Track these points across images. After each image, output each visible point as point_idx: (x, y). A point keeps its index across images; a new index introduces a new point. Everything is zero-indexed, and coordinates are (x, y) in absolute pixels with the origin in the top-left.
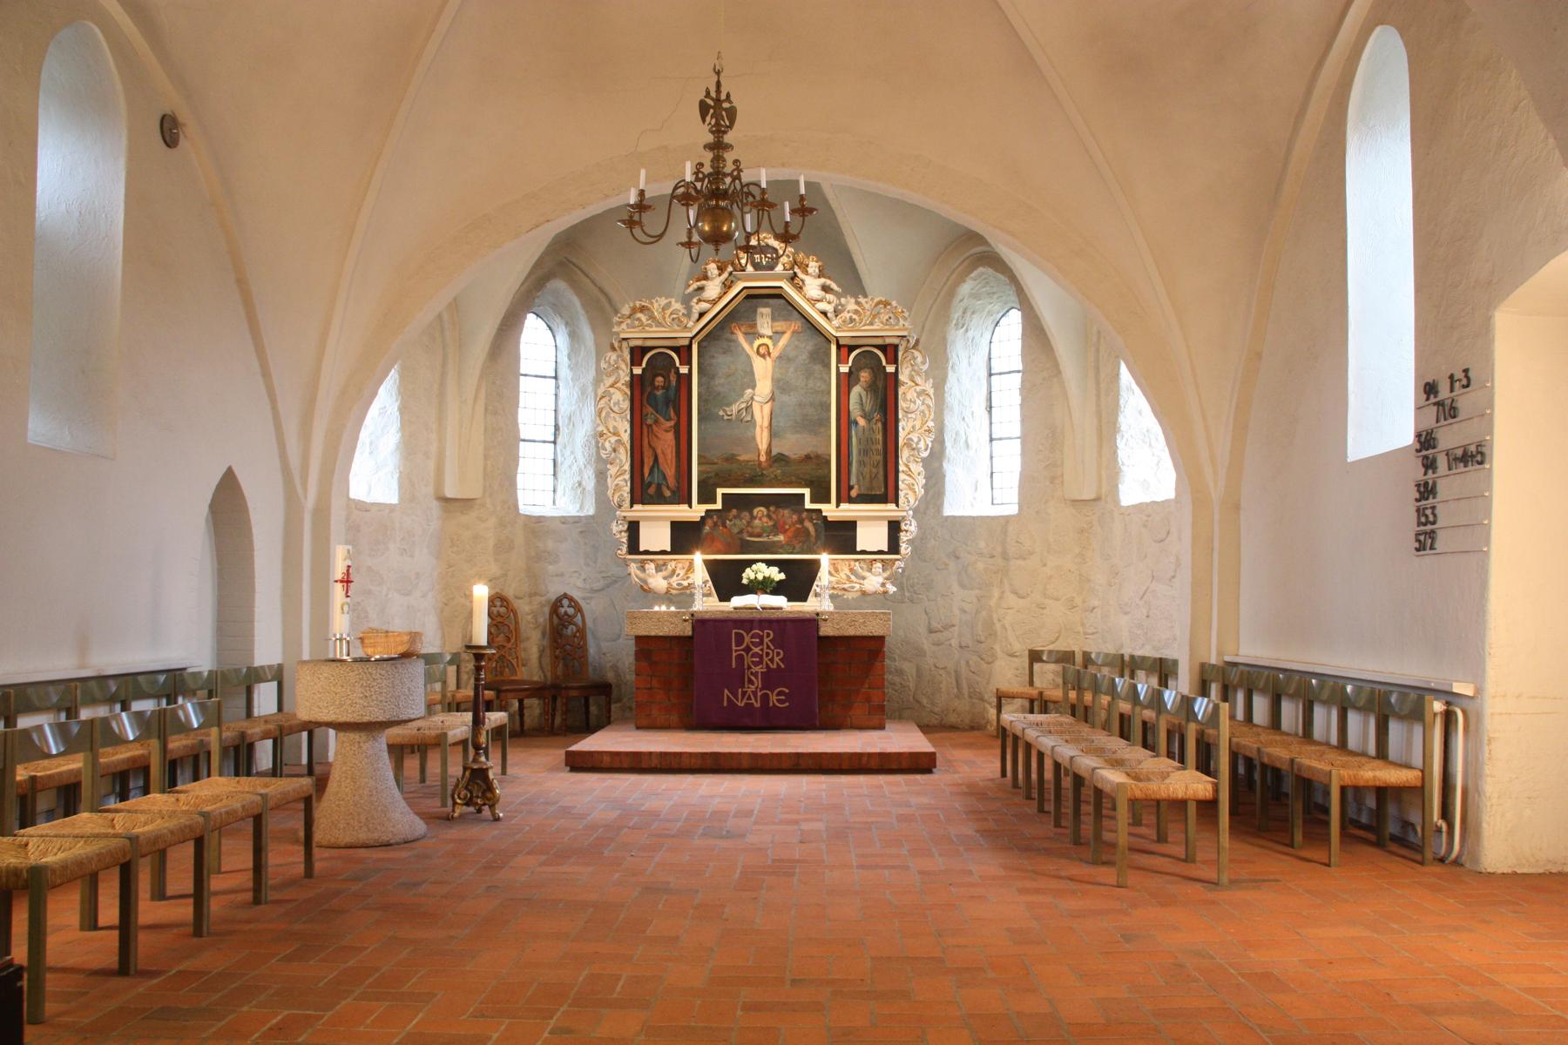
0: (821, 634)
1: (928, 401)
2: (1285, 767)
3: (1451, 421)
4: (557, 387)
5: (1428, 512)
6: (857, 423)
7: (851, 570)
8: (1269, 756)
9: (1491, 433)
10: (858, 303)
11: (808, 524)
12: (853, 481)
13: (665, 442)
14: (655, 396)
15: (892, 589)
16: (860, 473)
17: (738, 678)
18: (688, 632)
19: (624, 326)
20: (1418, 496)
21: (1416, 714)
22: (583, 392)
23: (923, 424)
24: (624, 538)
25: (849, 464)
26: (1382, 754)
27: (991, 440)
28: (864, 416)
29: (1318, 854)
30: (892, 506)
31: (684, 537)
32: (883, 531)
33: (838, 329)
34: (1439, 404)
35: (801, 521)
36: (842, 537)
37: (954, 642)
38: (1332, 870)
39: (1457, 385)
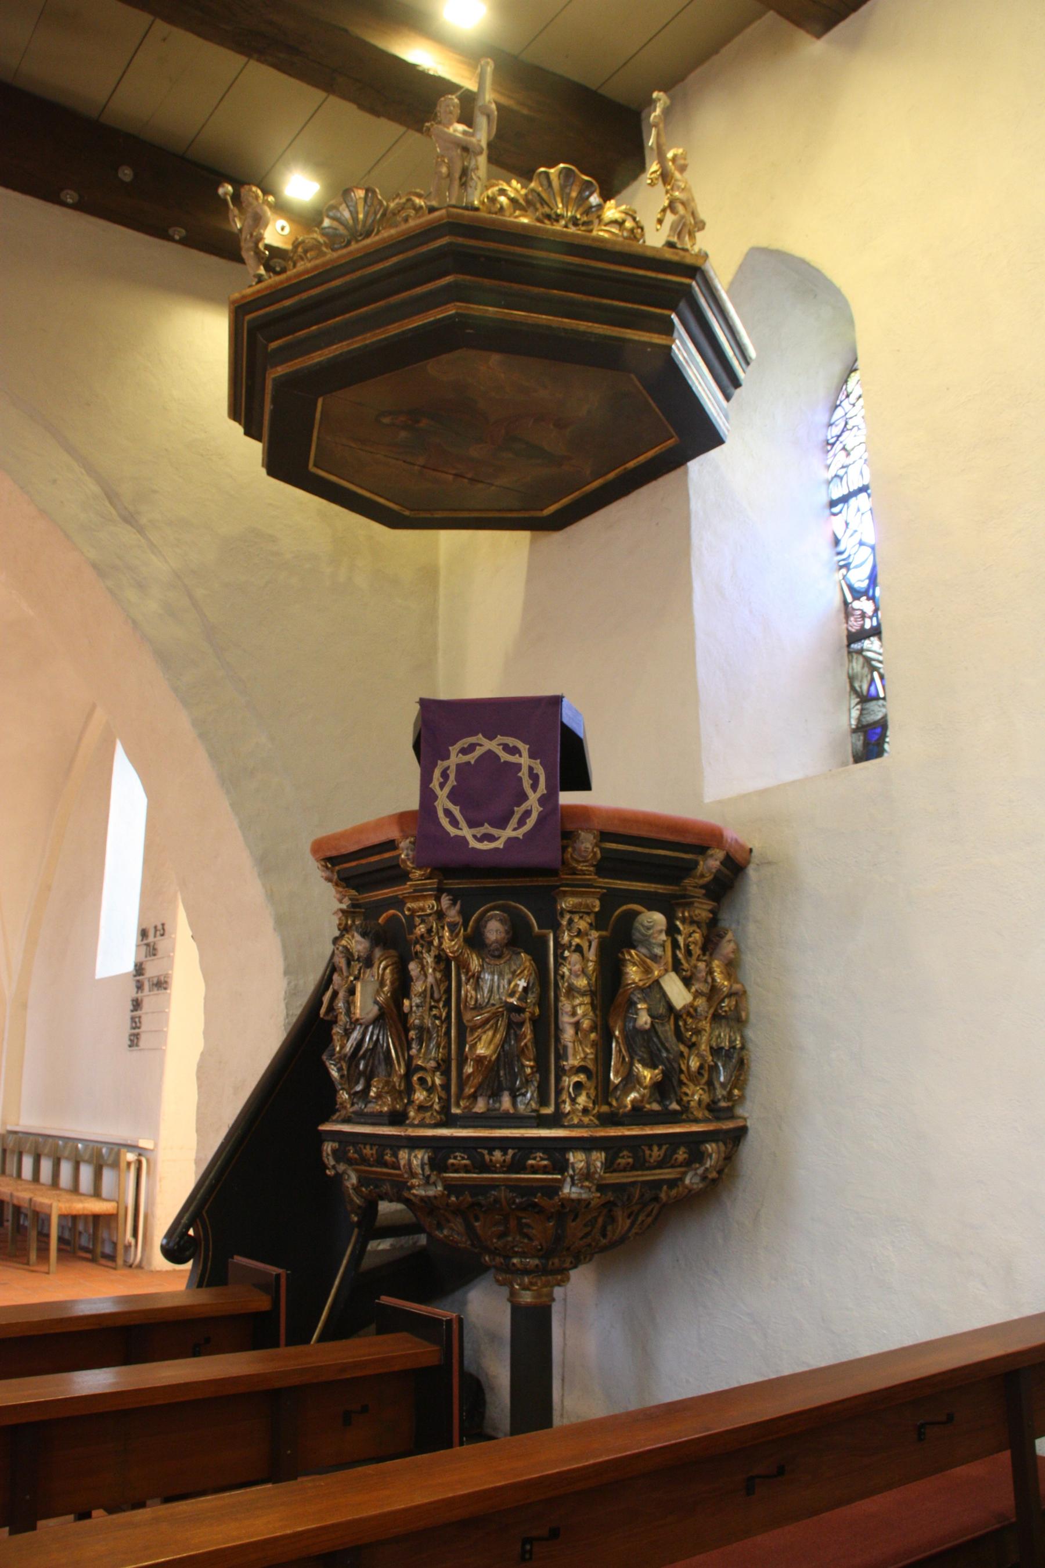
2: (26, 1205)
3: (153, 958)
5: (137, 1020)
8: (18, 1198)
21: (115, 1165)
26: (97, 1193)
29: (44, 1268)
34: (148, 945)
38: (50, 1277)
39: (158, 933)
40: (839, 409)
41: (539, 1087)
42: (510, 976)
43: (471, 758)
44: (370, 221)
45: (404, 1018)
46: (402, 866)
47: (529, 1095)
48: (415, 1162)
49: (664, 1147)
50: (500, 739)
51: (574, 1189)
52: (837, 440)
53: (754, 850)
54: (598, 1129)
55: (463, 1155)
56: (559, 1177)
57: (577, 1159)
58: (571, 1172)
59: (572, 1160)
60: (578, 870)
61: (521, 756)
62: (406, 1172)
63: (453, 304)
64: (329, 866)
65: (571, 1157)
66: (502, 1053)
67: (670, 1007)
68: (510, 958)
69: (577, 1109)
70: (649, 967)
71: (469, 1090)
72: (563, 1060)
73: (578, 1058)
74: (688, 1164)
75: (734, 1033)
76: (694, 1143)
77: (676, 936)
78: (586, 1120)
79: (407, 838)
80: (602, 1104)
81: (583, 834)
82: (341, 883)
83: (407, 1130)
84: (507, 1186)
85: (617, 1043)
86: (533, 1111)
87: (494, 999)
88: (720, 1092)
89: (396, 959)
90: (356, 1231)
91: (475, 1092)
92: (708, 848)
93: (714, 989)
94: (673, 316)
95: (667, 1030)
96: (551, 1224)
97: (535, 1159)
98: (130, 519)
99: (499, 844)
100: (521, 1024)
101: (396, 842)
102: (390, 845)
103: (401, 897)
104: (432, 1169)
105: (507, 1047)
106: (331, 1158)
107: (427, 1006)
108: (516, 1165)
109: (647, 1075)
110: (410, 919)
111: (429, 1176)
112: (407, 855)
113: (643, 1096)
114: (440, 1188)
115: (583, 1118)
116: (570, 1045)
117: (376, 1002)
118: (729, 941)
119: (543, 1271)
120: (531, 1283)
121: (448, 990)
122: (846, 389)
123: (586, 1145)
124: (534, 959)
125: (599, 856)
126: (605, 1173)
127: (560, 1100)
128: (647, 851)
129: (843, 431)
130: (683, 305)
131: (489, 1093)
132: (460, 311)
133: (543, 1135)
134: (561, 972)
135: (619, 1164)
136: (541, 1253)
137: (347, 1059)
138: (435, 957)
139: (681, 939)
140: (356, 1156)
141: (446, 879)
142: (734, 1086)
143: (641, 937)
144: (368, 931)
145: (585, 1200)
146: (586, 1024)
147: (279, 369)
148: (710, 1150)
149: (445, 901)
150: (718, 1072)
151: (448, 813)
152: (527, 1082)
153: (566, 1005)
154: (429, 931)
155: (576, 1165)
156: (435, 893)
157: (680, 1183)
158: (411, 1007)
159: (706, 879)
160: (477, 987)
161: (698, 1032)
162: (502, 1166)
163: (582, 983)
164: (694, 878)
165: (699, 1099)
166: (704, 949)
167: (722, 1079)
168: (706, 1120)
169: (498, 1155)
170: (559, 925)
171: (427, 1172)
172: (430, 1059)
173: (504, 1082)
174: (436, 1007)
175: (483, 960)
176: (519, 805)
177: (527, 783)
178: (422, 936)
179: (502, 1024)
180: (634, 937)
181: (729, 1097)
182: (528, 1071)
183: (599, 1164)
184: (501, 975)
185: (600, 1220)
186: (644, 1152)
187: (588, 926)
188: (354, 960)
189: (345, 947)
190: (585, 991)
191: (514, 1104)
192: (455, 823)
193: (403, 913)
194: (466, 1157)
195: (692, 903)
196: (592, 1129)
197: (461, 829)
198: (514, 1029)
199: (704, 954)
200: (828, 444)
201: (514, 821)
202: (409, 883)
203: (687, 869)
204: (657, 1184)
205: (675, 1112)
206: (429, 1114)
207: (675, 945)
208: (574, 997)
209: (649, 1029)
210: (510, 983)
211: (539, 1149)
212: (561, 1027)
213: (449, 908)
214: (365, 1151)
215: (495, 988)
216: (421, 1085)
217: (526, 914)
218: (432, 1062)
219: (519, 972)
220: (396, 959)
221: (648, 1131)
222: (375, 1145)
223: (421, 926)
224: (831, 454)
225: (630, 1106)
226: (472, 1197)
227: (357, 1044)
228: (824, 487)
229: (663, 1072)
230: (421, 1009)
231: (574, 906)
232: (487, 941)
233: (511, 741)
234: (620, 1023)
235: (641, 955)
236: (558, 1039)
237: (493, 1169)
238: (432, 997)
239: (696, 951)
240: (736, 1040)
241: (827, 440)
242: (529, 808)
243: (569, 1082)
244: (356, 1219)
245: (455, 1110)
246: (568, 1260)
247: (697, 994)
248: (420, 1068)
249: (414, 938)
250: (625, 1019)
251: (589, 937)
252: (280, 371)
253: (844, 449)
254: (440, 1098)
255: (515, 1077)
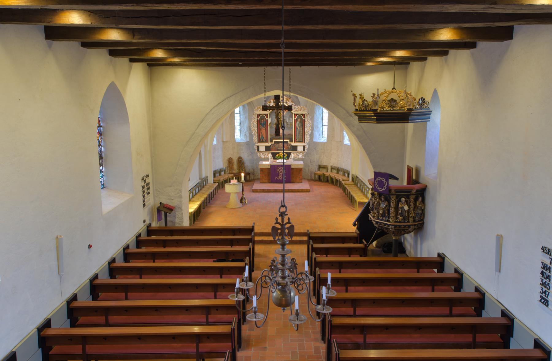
0: (292, 167)
1: (310, 124)
4: (240, 115)
6: (297, 128)
7: (296, 154)
10: (298, 107)
11: (289, 146)
12: (297, 139)
13: (264, 131)
14: (262, 123)
15: (303, 157)
16: (298, 137)
17: (278, 175)
18: (270, 167)
19: (256, 111)
22: (246, 118)
23: (309, 128)
24: (257, 149)
25: (296, 136)
27: (323, 125)
28: (299, 127)
30: (304, 143)
31: (268, 149)
32: (302, 147)
33: (294, 112)
35: (288, 146)
36: (295, 148)
37: (315, 164)
43: (379, 180)
65: (390, 226)
67: (405, 210)
99: (382, 190)
151: (377, 186)
152: (387, 216)
153: (391, 209)
201: (383, 188)
203: (411, 192)
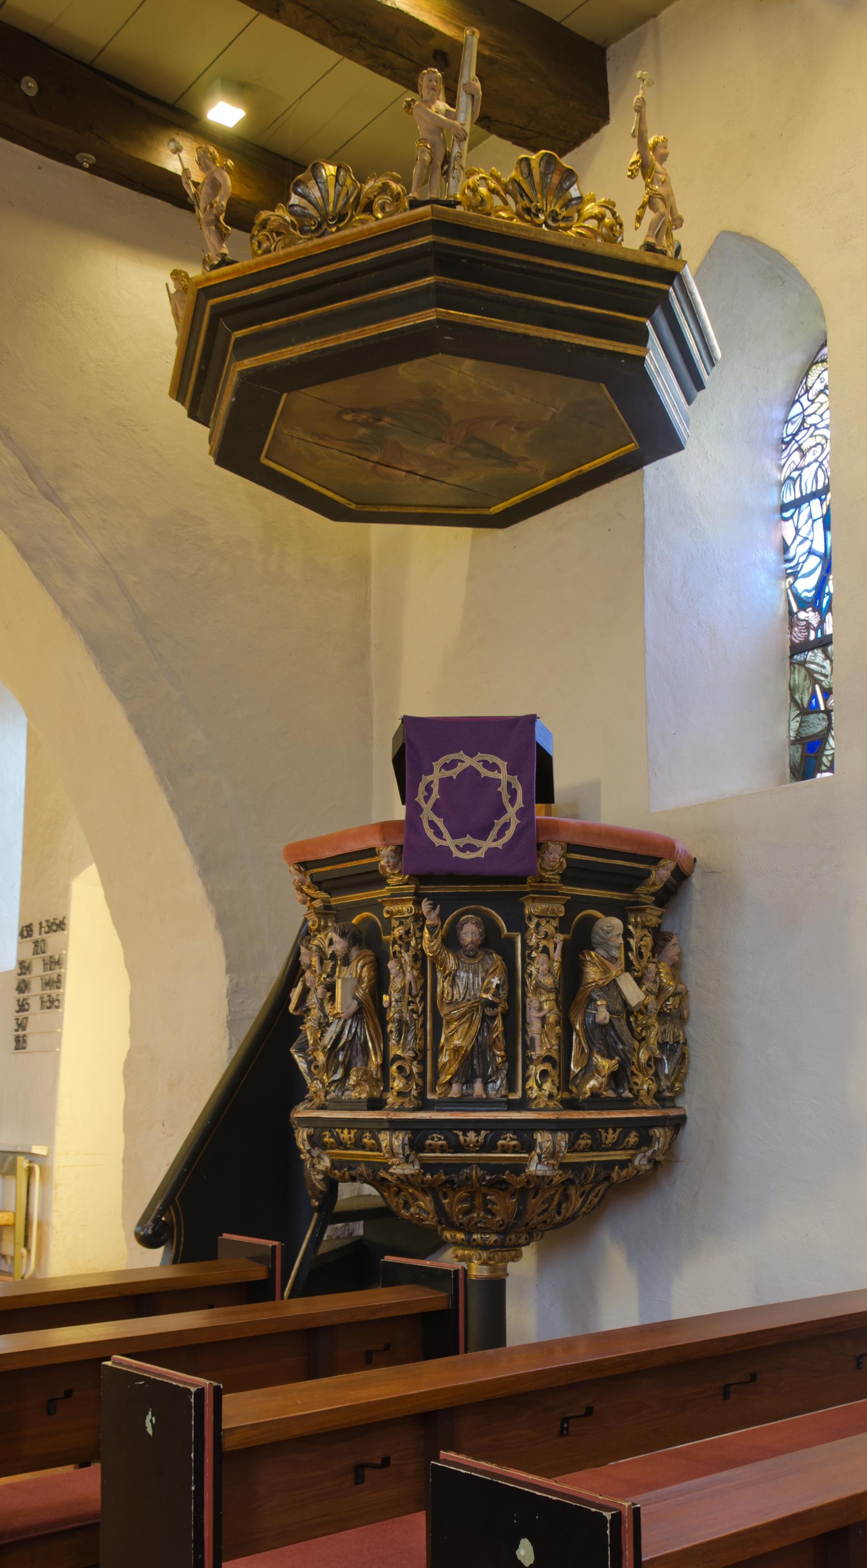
9: (66, 947)
20: (16, 1027)
40: (798, 405)
41: (507, 1075)
42: (484, 974)
43: (454, 773)
44: (341, 203)
45: (381, 1013)
46: (381, 872)
47: (499, 1083)
48: (396, 1143)
49: (618, 1131)
50: (480, 756)
51: (539, 1167)
52: (793, 439)
53: (698, 860)
54: (563, 1112)
55: (439, 1136)
56: (526, 1155)
57: (543, 1139)
58: (538, 1151)
59: (539, 1139)
60: (545, 879)
61: (499, 772)
62: (387, 1152)
63: (433, 310)
64: (303, 870)
65: (539, 1137)
66: (476, 1044)
67: (625, 1004)
68: (483, 958)
69: (544, 1095)
70: (607, 968)
71: (445, 1078)
72: (531, 1051)
73: (545, 1048)
74: (637, 1147)
75: (678, 1030)
76: (644, 1127)
77: (629, 939)
78: (551, 1104)
79: (388, 847)
80: (563, 1092)
81: (552, 846)
82: (315, 886)
83: (388, 1114)
84: (479, 1165)
85: (577, 1035)
86: (503, 1096)
87: (470, 995)
88: (665, 1083)
89: (372, 958)
90: (316, 1215)
91: (451, 1079)
92: (661, 859)
93: (661, 989)
94: (648, 324)
95: (621, 1025)
96: (514, 1200)
97: (505, 1139)
98: (51, 496)
99: (480, 854)
100: (494, 1018)
101: (377, 849)
102: (371, 852)
103: (380, 900)
104: (411, 1149)
105: (480, 1038)
106: (306, 1143)
107: (406, 1001)
108: (489, 1146)
109: (605, 1065)
110: (387, 922)
111: (408, 1156)
112: (388, 862)
113: (601, 1084)
114: (417, 1167)
115: (549, 1103)
116: (537, 1037)
117: (355, 998)
118: (675, 945)
119: (500, 1246)
120: (489, 1259)
121: (424, 987)
122: (806, 383)
123: (553, 1126)
124: (504, 960)
125: (565, 866)
126: (568, 1152)
127: (527, 1087)
128: (606, 861)
129: (799, 430)
130: (658, 313)
131: (464, 1080)
132: (440, 317)
133: (513, 1118)
134: (528, 971)
135: (580, 1145)
136: (503, 1228)
137: (326, 1050)
138: (413, 956)
139: (632, 942)
140: (332, 1140)
141: (422, 885)
142: (676, 1080)
143: (600, 940)
144: (347, 931)
145: (549, 1177)
146: (552, 1018)
147: (246, 362)
148: (658, 1134)
149: (425, 906)
150: (663, 1065)
151: (432, 824)
152: (497, 1071)
153: (533, 1001)
154: (407, 932)
155: (543, 1145)
156: (414, 897)
157: (629, 1164)
158: (391, 1002)
159: (656, 887)
160: (453, 984)
161: (647, 1027)
162: (475, 1146)
163: (548, 981)
164: (646, 886)
165: (648, 1088)
166: (653, 951)
167: (666, 1071)
168: (655, 1108)
169: (472, 1136)
170: (527, 928)
171: (407, 1152)
172: (409, 1050)
173: (477, 1070)
174: (413, 1002)
175: (459, 959)
176: (498, 818)
177: (506, 798)
178: (401, 937)
179: (477, 1017)
180: (593, 940)
181: (671, 1088)
182: (499, 1060)
183: (563, 1144)
184: (475, 973)
185: (557, 1198)
186: (600, 1134)
187: (553, 929)
188: (326, 959)
189: (317, 946)
190: (551, 989)
191: (485, 1090)
192: (439, 834)
193: (380, 916)
194: (442, 1138)
195: (645, 909)
196: (557, 1112)
197: (445, 840)
198: (487, 1023)
199: (654, 957)
200: (783, 442)
201: (494, 833)
202: (387, 888)
203: (641, 877)
204: (609, 1165)
205: (628, 1099)
206: (407, 1099)
207: (628, 947)
208: (541, 994)
209: (607, 1024)
210: (483, 980)
211: (508, 1130)
212: (528, 1021)
213: (429, 912)
214: (342, 1136)
215: (471, 986)
216: (400, 1073)
217: (496, 917)
218: (410, 1052)
219: (491, 970)
220: (372, 958)
221: (605, 1115)
222: (353, 1129)
223: (399, 928)
224: (786, 453)
225: (589, 1094)
226: (446, 1174)
227: (336, 1036)
228: (775, 489)
229: (619, 1062)
230: (399, 1003)
231: (542, 911)
232: (462, 942)
233: (491, 758)
234: (580, 1018)
235: (600, 956)
236: (525, 1032)
237: (467, 1148)
238: (410, 993)
239: (647, 953)
240: (679, 1036)
241: (783, 438)
242: (508, 821)
243: (536, 1070)
244: (317, 1204)
245: (430, 1096)
246: (523, 1237)
247: (648, 992)
248: (397, 1058)
249: (392, 939)
250: (585, 1014)
251: (555, 940)
252: (248, 363)
253: (799, 449)
254: (417, 1085)
255: (486, 1065)
